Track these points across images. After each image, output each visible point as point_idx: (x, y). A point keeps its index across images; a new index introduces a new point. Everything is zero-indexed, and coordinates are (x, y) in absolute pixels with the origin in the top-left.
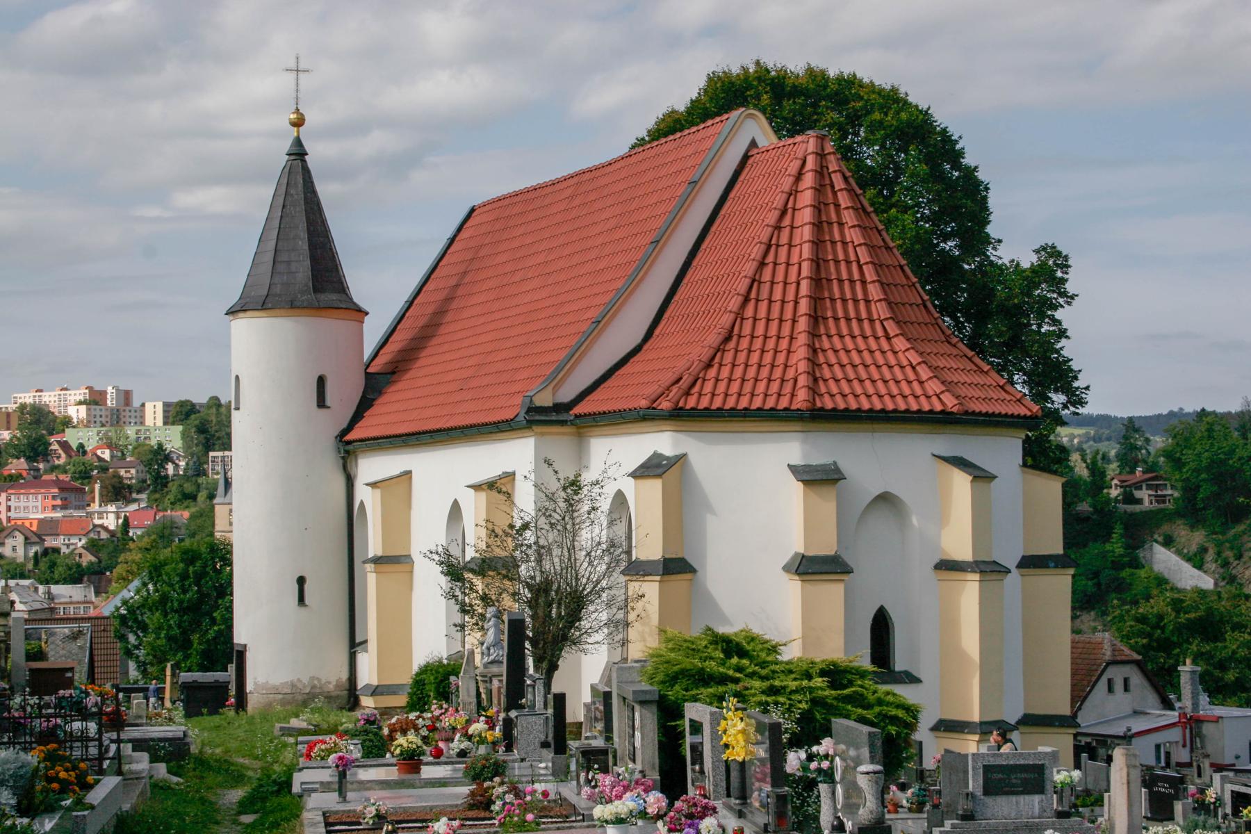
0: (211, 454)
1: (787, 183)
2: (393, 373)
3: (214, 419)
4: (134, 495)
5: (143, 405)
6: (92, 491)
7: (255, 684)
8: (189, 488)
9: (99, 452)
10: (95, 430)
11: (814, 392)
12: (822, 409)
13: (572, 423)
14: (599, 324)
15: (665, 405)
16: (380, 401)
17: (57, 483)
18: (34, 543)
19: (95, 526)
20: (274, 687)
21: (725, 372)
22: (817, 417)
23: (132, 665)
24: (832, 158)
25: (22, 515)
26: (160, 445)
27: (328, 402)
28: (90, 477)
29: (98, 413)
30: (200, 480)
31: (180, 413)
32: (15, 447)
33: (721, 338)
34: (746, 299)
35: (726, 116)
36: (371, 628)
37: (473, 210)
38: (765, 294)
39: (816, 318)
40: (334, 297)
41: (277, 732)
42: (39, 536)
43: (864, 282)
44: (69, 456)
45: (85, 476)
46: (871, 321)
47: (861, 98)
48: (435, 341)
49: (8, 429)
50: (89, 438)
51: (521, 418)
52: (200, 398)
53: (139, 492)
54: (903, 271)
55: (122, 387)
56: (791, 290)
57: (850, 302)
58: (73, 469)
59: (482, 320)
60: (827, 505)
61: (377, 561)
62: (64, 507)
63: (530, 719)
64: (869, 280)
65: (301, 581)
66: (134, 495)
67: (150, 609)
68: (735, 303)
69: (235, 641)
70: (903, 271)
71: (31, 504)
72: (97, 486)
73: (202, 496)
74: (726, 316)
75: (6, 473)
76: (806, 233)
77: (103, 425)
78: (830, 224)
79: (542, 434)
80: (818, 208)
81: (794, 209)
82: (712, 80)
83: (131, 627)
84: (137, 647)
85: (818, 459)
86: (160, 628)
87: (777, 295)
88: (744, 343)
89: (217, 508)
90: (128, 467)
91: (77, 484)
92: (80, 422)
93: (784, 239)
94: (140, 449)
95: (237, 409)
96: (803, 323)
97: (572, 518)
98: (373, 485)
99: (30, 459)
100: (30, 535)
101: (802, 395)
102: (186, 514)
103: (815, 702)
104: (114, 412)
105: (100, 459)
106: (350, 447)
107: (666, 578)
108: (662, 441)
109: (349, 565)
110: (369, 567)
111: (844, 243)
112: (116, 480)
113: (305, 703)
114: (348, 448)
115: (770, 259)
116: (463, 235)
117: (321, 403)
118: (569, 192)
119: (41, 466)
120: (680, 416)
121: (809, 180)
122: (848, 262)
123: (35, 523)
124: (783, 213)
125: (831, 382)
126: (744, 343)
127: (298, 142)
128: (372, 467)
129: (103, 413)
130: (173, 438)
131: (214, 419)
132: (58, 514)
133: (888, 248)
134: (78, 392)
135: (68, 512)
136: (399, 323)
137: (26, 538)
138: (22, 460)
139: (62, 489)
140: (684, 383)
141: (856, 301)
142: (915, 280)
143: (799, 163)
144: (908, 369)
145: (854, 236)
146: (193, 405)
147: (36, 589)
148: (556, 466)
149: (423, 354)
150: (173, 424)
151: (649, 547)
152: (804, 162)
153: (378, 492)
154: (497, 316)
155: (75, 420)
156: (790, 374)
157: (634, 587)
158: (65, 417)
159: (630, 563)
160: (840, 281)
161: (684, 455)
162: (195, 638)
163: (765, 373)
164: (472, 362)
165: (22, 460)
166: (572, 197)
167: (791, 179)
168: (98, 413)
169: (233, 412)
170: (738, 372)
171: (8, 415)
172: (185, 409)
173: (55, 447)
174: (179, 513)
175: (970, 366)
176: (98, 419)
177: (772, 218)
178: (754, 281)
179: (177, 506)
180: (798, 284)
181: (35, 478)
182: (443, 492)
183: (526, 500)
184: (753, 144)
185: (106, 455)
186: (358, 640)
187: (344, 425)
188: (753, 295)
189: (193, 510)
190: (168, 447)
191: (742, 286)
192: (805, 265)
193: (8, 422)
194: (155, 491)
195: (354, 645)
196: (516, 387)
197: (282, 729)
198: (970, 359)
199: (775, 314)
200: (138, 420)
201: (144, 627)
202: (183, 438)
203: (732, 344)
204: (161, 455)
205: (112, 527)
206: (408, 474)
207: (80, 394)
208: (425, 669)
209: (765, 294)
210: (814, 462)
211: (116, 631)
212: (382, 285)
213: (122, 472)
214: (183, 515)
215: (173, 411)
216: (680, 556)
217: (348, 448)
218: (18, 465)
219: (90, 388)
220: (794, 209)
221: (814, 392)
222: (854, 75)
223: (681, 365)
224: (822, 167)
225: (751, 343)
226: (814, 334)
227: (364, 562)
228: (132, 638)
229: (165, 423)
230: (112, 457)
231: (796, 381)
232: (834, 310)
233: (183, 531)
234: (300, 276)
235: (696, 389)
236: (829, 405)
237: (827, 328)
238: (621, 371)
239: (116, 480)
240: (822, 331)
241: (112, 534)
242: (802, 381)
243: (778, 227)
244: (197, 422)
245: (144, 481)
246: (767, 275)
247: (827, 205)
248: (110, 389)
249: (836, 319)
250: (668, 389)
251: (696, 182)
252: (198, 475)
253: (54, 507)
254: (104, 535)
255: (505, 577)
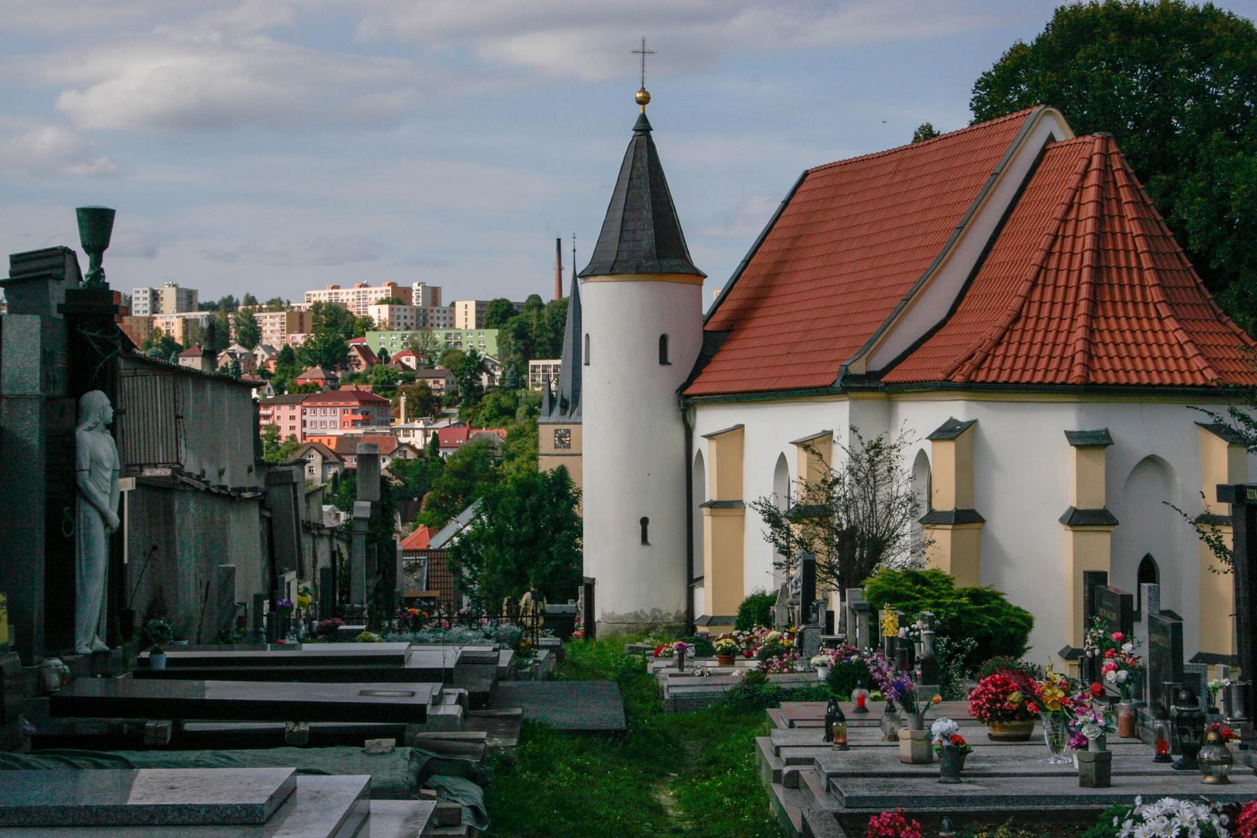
0: (532, 363)
1: (1074, 180)
2: (730, 331)
3: (534, 321)
4: (444, 410)
5: (453, 305)
6: (397, 404)
7: (603, 614)
8: (506, 401)
9: (404, 359)
10: (400, 333)
11: (1089, 368)
12: (1094, 383)
13: (882, 389)
14: (908, 301)
15: (958, 378)
16: (718, 357)
17: (358, 395)
18: (333, 464)
19: (401, 445)
20: (620, 617)
21: (1012, 351)
22: (1087, 390)
23: (466, 600)
24: (1115, 157)
25: (319, 431)
26: (474, 352)
27: (670, 359)
28: (395, 388)
29: (402, 314)
30: (519, 393)
31: (495, 314)
32: (310, 352)
33: (1010, 319)
34: (1034, 285)
35: (1028, 111)
36: (707, 564)
37: (806, 174)
38: (1050, 281)
39: (1095, 302)
40: (674, 262)
41: (626, 651)
42: (338, 456)
43: (1140, 269)
44: (370, 363)
45: (388, 386)
46: (1146, 304)
47: (1213, 35)
48: (770, 302)
49: (301, 331)
50: (390, 342)
51: (837, 385)
52: (518, 296)
53: (449, 405)
54: (1179, 258)
55: (430, 284)
56: (1074, 276)
57: (1127, 288)
58: (375, 378)
59: (810, 286)
60: (1097, 464)
61: (713, 505)
62: (365, 423)
63: (814, 631)
64: (1145, 267)
65: (644, 522)
66: (444, 410)
67: (486, 543)
68: (1023, 289)
69: (585, 575)
70: (1179, 258)
71: (328, 419)
72: (403, 399)
73: (521, 411)
74: (1016, 299)
75: (300, 383)
76: (1089, 226)
77: (408, 328)
78: (1112, 217)
79: (856, 399)
80: (1101, 203)
81: (1079, 204)
82: (1060, 14)
83: (465, 561)
84: (471, 582)
85: (1091, 426)
86: (496, 562)
87: (1062, 281)
88: (1031, 324)
89: (542, 428)
90: (436, 377)
91: (379, 396)
92: (382, 323)
93: (1070, 231)
94: (451, 356)
95: (587, 364)
96: (1083, 307)
97: (874, 477)
98: (710, 437)
99: (326, 367)
100: (328, 454)
101: (1077, 371)
102: (504, 432)
103: (962, 612)
104: (420, 312)
105: (406, 368)
106: (689, 401)
107: (957, 527)
108: (956, 409)
109: (686, 511)
110: (706, 511)
111: (1124, 234)
112: (423, 392)
113: (646, 633)
114: (687, 403)
115: (1057, 248)
116: (796, 199)
117: (663, 360)
118: (891, 168)
119: (339, 375)
120: (972, 388)
121: (1093, 178)
122: (1127, 252)
123: (334, 441)
124: (1070, 207)
125: (1105, 360)
126: (1031, 324)
127: (643, 119)
128: (710, 420)
129: (408, 314)
130: (487, 344)
131: (534, 321)
132: (359, 431)
133: (1165, 237)
134: (379, 289)
135: (370, 428)
136: (735, 282)
137: (324, 458)
138: (318, 368)
139: (363, 402)
140: (978, 357)
141: (1132, 286)
142: (1190, 265)
143: (1085, 162)
144: (1176, 348)
145: (1133, 227)
146: (510, 305)
147: (338, 516)
148: (860, 432)
149: (757, 315)
150: (487, 327)
151: (945, 501)
152: (1090, 161)
153: (714, 443)
154: (824, 283)
155: (376, 322)
156: (1069, 352)
157: (928, 534)
158: (365, 318)
159: (931, 511)
160: (1119, 268)
161: (975, 421)
162: (531, 572)
163: (1047, 350)
164: (799, 327)
165: (318, 368)
166: (895, 173)
167: (1078, 177)
168: (402, 314)
169: (583, 367)
170: (1051, 337)
171: (301, 315)
172: (500, 310)
173: (355, 352)
174: (495, 431)
175: (1236, 342)
176: (402, 321)
177: (1059, 212)
178: (1041, 268)
179: (493, 423)
180: (1080, 271)
181: (333, 388)
182: (771, 446)
183: (839, 461)
184: (1051, 138)
185: (412, 362)
186: (695, 576)
187: (684, 380)
188: (1040, 281)
189: (511, 427)
190: (482, 353)
191: (1031, 274)
192: (1087, 254)
193: (301, 324)
194: (467, 405)
195: (692, 581)
196: (835, 356)
197: (631, 648)
198: (1238, 336)
199: (1059, 298)
200: (447, 322)
201: (478, 560)
202: (498, 344)
203: (1020, 325)
204: (475, 364)
205: (419, 446)
206: (740, 428)
207: (383, 291)
208: (753, 600)
209: (1050, 281)
210: (1089, 428)
211: (451, 564)
212: (718, 252)
213: (430, 383)
214: (497, 434)
215: (487, 311)
216: (970, 507)
217: (687, 403)
218: (313, 374)
219: (393, 285)
220: (1079, 204)
221: (1089, 368)
222: (1211, 7)
223: (976, 341)
224: (1106, 166)
225: (1037, 323)
226: (1092, 316)
227: (702, 506)
228: (466, 572)
229: (478, 326)
230: (418, 364)
231: (1073, 358)
232: (1112, 295)
233: (499, 452)
234: (644, 243)
235: (986, 364)
236: (1101, 379)
237: (1104, 310)
238: (914, 355)
239: (423, 392)
240: (1100, 313)
241: (420, 453)
242: (1079, 358)
243: (1064, 220)
244: (515, 326)
245: (455, 393)
246: (1053, 264)
247: (1109, 200)
248: (415, 286)
249: (1114, 303)
250: (963, 364)
251: (997, 174)
252: (516, 387)
253: (354, 423)
254: (411, 455)
255: (818, 524)
